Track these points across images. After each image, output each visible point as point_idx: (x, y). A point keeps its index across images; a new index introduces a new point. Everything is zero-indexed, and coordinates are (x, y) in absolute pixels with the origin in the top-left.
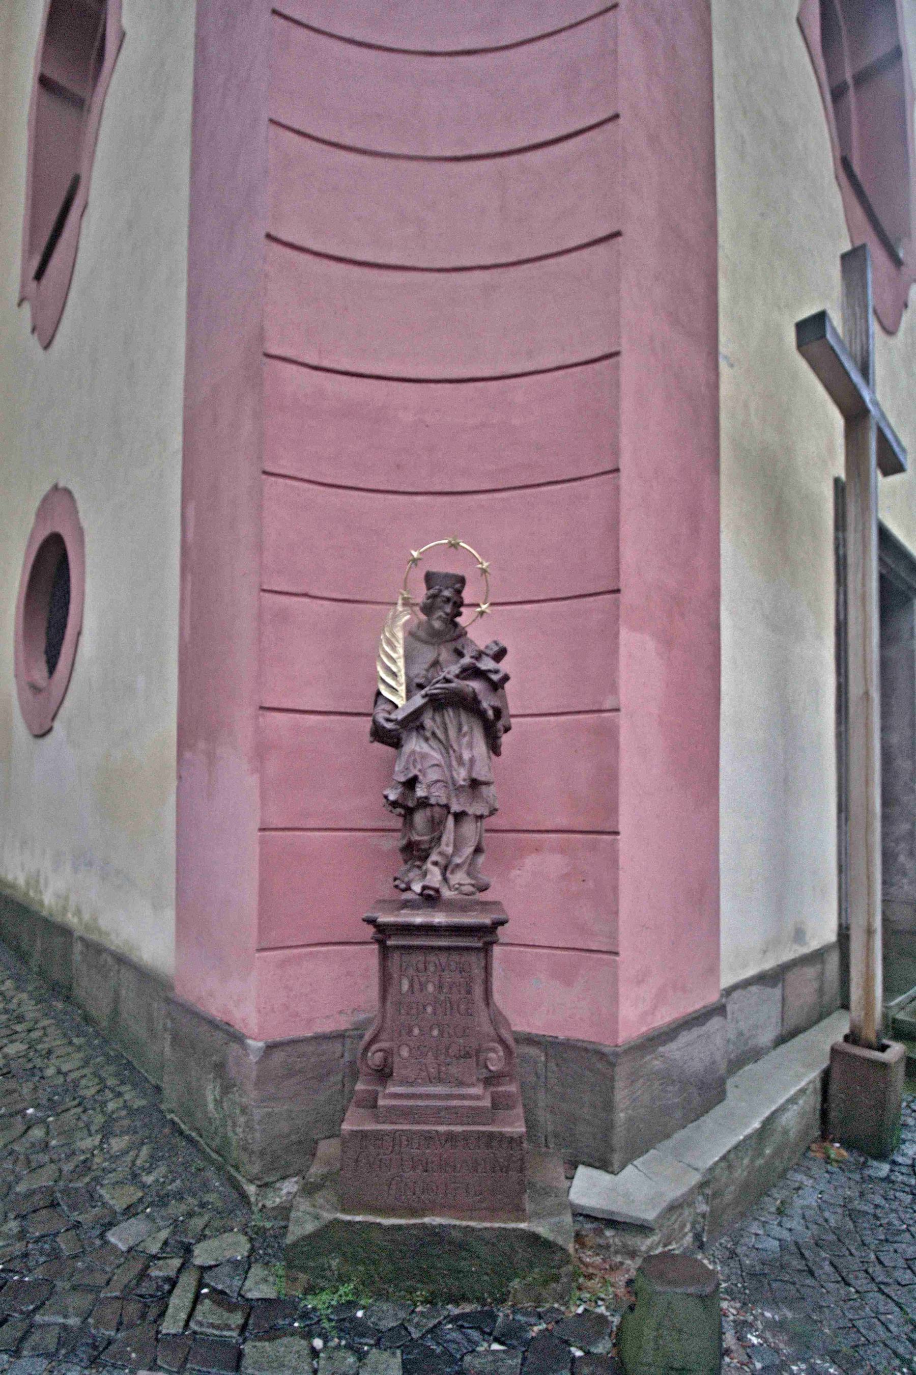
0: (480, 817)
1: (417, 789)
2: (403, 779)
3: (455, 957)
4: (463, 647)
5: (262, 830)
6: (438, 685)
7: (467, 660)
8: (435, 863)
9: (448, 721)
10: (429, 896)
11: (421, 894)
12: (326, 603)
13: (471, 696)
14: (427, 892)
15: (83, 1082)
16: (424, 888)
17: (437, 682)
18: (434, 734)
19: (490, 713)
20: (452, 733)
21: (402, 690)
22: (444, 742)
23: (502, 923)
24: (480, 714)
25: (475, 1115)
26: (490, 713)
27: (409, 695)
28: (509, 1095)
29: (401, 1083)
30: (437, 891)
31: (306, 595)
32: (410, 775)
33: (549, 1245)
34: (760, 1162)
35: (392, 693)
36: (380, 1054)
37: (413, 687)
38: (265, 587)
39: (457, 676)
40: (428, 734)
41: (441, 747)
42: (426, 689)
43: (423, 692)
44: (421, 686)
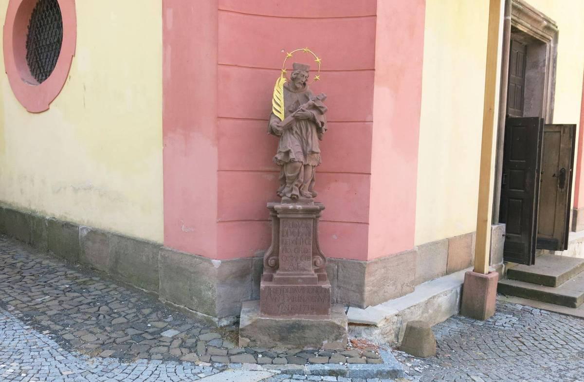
0: (314, 166)
1: (290, 155)
2: (284, 151)
3: (304, 221)
4: (308, 95)
5: (218, 171)
6: (299, 113)
7: (311, 102)
8: (297, 185)
9: (163, 344)
10: (294, 198)
11: (291, 198)
12: (245, 69)
13: (312, 117)
14: (293, 197)
15: (162, 254)
16: (292, 195)
17: (299, 111)
18: (296, 132)
19: (320, 124)
20: (304, 132)
21: (283, 112)
22: (300, 135)
23: (323, 209)
24: (316, 125)
25: (312, 280)
26: (320, 124)
27: (285, 117)
28: (324, 275)
29: (283, 271)
30: (297, 196)
31: (236, 65)
32: (287, 150)
33: (339, 327)
34: (426, 315)
35: (279, 113)
36: (273, 260)
37: (288, 111)
38: (219, 63)
39: (307, 109)
40: (294, 132)
41: (299, 137)
42: (294, 113)
43: (292, 115)
44: (291, 112)
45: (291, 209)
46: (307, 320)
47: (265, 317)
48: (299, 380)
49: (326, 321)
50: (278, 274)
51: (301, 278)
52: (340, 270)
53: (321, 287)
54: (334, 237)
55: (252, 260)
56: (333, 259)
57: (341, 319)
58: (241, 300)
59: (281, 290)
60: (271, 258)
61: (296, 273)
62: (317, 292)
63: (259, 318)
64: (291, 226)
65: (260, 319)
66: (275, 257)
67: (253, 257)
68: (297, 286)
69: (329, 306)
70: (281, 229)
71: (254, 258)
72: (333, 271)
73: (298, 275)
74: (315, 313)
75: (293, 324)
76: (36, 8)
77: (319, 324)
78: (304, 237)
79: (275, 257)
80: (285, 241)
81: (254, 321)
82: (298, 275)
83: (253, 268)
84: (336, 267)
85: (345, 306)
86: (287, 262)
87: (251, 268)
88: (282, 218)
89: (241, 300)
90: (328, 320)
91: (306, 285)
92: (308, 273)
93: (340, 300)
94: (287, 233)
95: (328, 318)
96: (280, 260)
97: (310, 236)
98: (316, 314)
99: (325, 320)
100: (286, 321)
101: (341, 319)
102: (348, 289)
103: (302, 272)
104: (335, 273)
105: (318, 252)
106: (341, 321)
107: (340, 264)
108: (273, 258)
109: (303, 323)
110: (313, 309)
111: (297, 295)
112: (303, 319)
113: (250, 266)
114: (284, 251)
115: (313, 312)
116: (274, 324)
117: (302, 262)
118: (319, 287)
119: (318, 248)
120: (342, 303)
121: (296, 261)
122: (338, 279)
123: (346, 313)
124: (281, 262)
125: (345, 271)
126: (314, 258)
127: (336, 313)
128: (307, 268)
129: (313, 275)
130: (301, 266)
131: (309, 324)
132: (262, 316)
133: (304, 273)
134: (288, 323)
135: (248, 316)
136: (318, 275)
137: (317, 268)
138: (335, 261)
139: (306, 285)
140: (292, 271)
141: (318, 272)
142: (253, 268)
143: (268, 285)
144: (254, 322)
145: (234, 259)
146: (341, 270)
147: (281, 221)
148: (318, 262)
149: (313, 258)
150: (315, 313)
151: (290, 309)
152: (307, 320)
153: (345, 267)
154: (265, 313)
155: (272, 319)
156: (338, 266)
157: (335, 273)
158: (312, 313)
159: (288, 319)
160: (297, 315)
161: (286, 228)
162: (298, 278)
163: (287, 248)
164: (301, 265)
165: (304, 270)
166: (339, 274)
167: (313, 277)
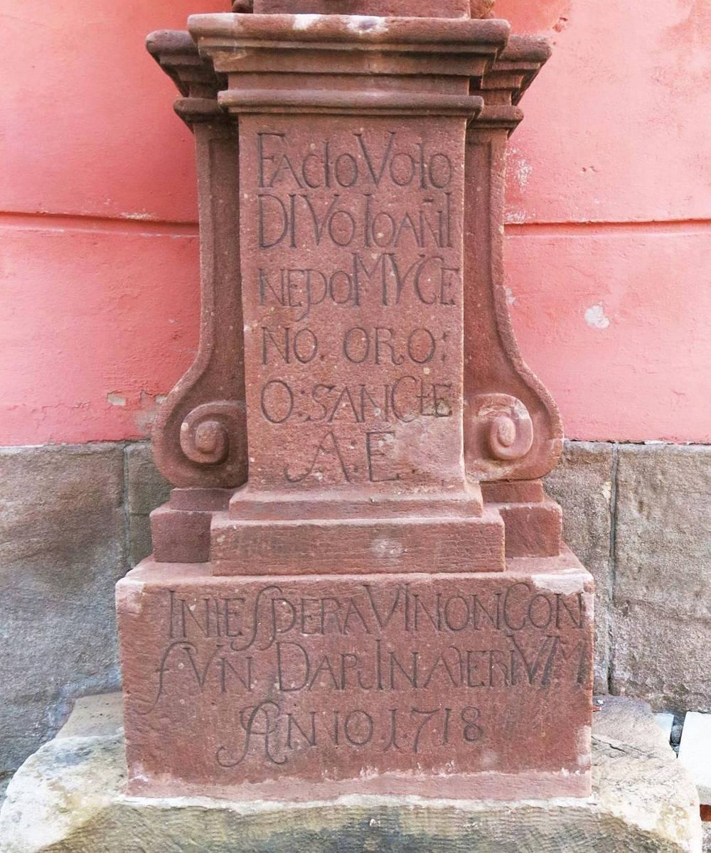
3: (410, 139)
36: (215, 424)
45: (302, 33)
46: (439, 804)
47: (158, 792)
48: (609, 441)
49: (561, 810)
50: (246, 509)
51: (395, 533)
52: (630, 510)
53: (528, 584)
54: (594, 316)
55: (123, 455)
56: (588, 446)
57: (660, 791)
58: (68, 688)
59: (256, 609)
60: (195, 412)
61: (359, 496)
62: (501, 618)
63: (121, 798)
64: (316, 168)
65: (122, 808)
66: (220, 404)
67: (128, 441)
68: (367, 585)
69: (582, 713)
70: (245, 196)
71: (130, 448)
72: (591, 514)
73: (372, 508)
74: (488, 758)
75: (346, 831)
76: (682, 822)
77: (520, 832)
78: (410, 254)
79: (220, 404)
80: (274, 279)
81: (80, 821)
82: (372, 508)
83: (128, 508)
84: (607, 491)
85: (657, 710)
86: (295, 421)
87: (121, 503)
88: (256, 109)
89: (68, 688)
90: (582, 803)
91: (426, 578)
92: (446, 497)
93: (627, 676)
94: (291, 224)
95: (575, 788)
96: (252, 412)
97: (446, 241)
98: (500, 766)
99: (558, 802)
100: (299, 815)
101: (660, 791)
102: (676, 617)
103: (397, 495)
104: (602, 525)
105: (503, 370)
106: (658, 807)
107: (627, 473)
108: (204, 407)
109: (413, 827)
110: (472, 731)
111: (372, 645)
112: (414, 800)
113: (112, 493)
114: (273, 350)
115: (478, 751)
116: (221, 834)
117: (401, 427)
118: (513, 586)
119: (500, 338)
120: (638, 689)
121: (360, 418)
122: (615, 559)
123: (675, 742)
124: (257, 429)
125: (657, 513)
126: (479, 404)
127: (622, 751)
128: (428, 467)
129: (472, 508)
130: (396, 454)
131: (453, 832)
132: (136, 788)
133: (418, 494)
134: (314, 826)
135: (54, 786)
136: (504, 514)
137: (498, 472)
138: (600, 457)
139: (426, 578)
140: (333, 482)
141: (504, 501)
142: (128, 508)
143: (170, 582)
144: (88, 830)
145: (12, 450)
146: (633, 505)
147: (247, 132)
148: (507, 427)
149: (474, 404)
150: (488, 758)
151: (324, 737)
152: (439, 804)
153: (654, 488)
154: (156, 767)
155: (209, 803)
156: (616, 485)
157: (599, 523)
158: (468, 762)
159: (311, 804)
160: (371, 774)
161: (288, 186)
162: (375, 532)
163: (295, 327)
164: (393, 443)
165: (417, 477)
166: (622, 527)
167: (473, 519)
